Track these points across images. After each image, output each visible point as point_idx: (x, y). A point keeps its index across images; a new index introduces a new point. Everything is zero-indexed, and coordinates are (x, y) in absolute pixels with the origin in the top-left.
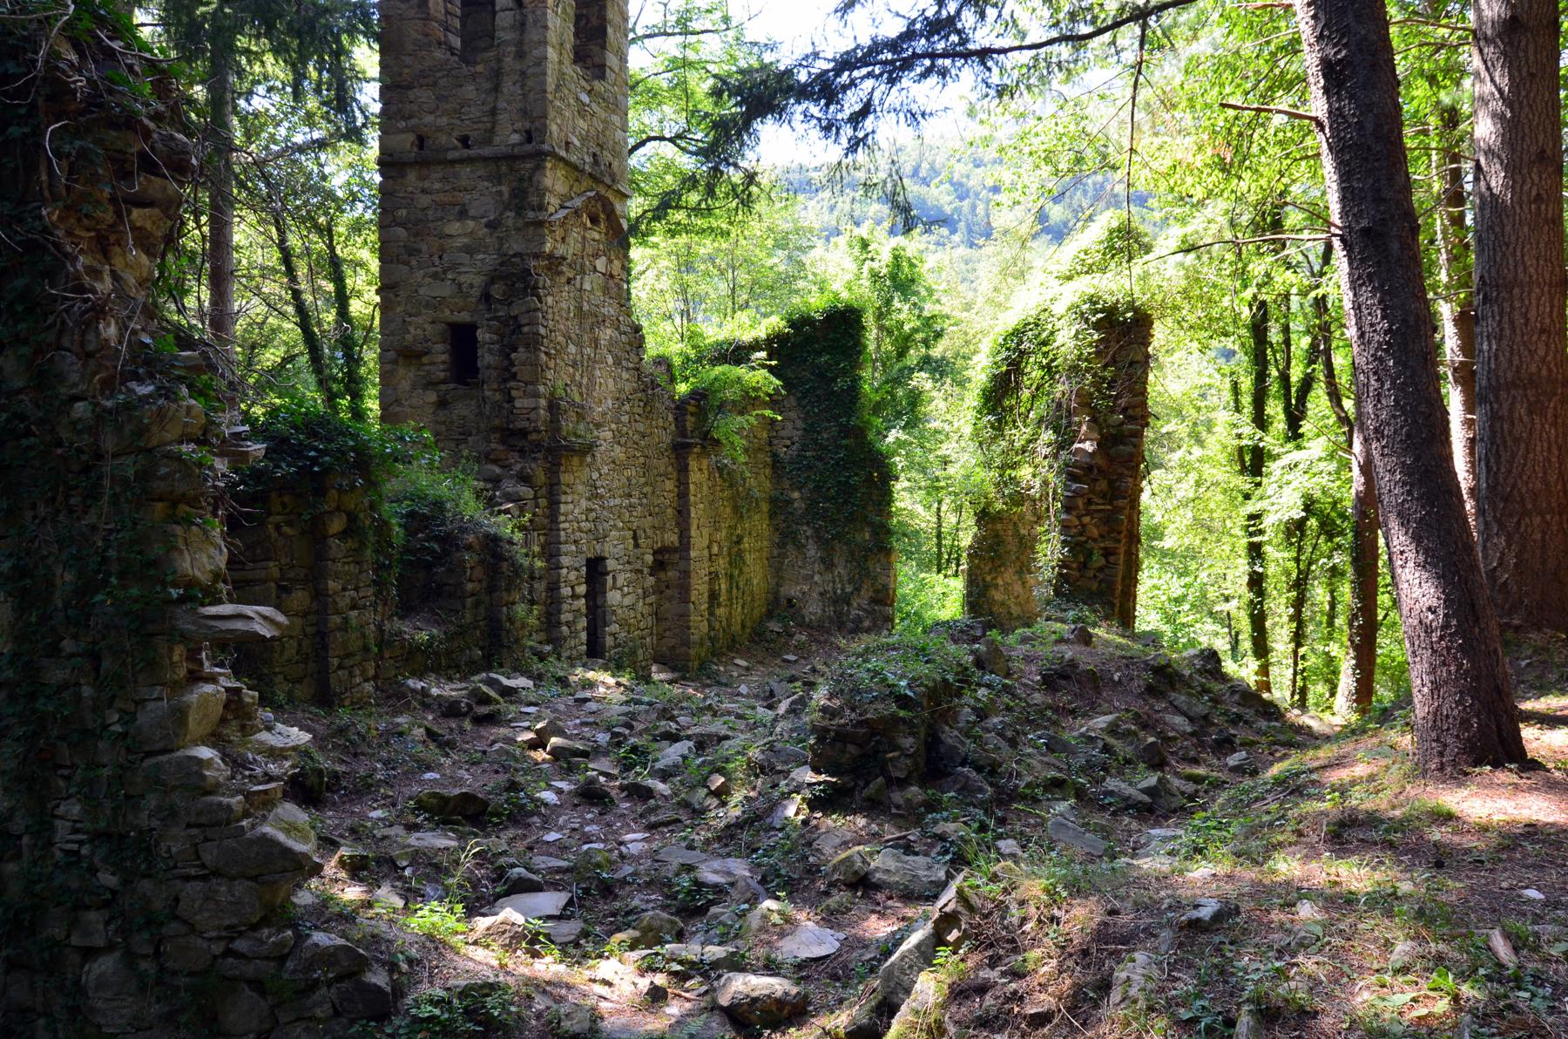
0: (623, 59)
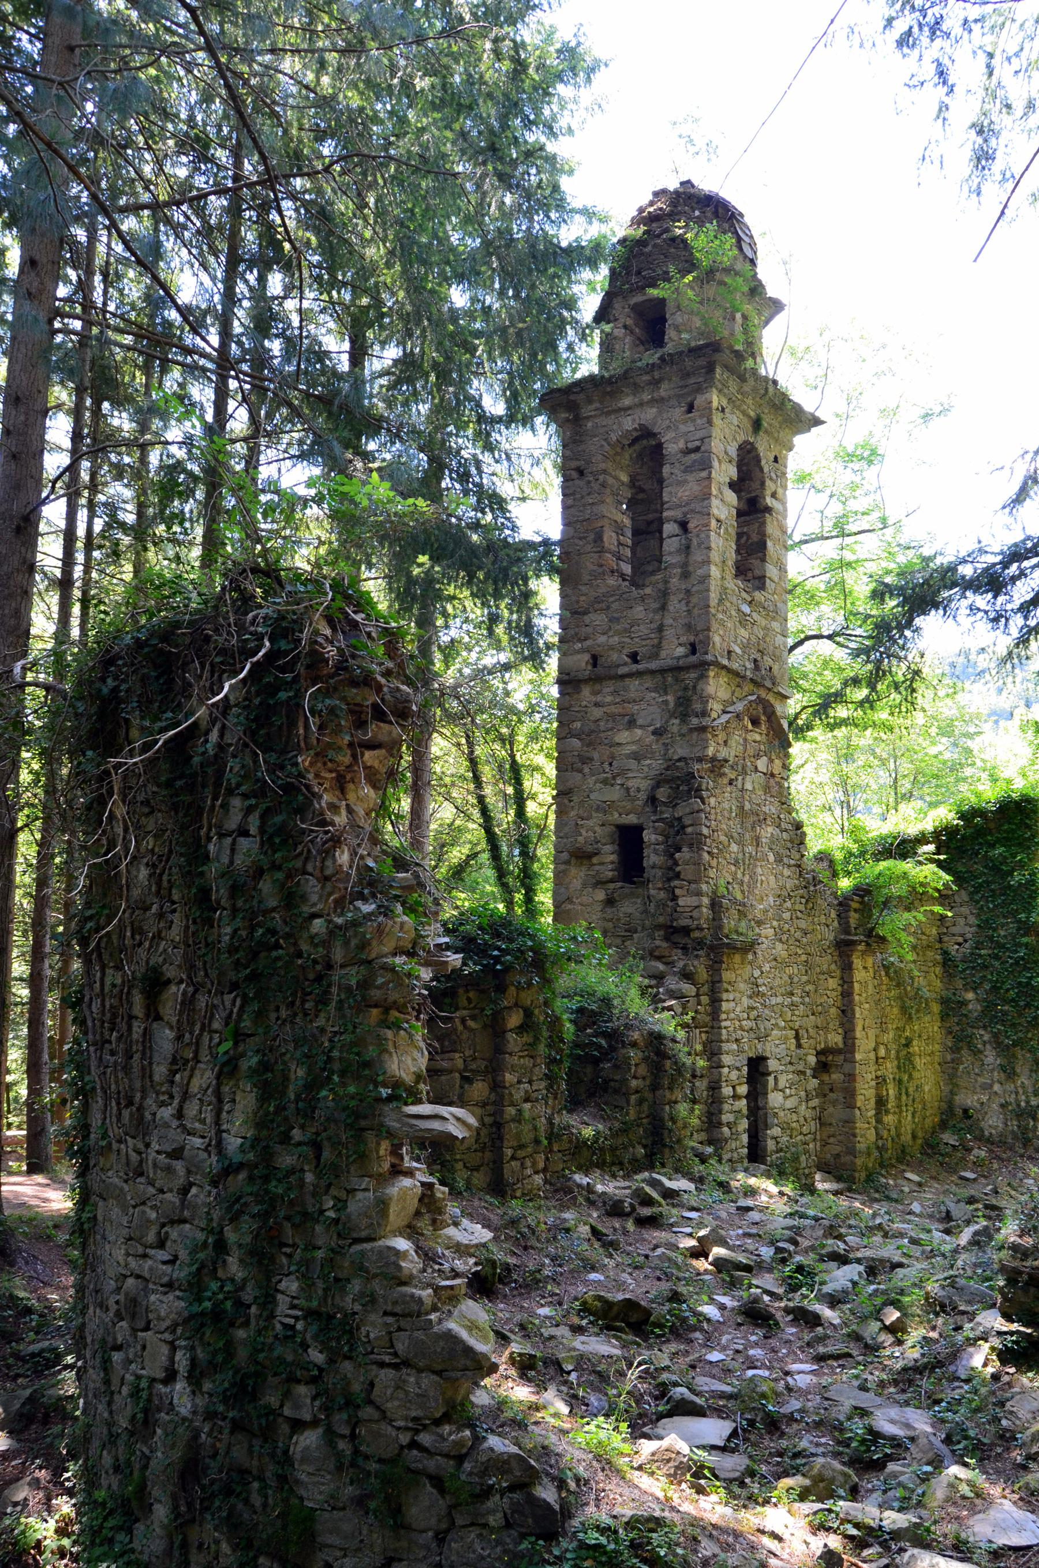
0: (783, 569)
